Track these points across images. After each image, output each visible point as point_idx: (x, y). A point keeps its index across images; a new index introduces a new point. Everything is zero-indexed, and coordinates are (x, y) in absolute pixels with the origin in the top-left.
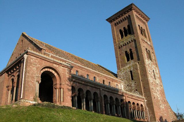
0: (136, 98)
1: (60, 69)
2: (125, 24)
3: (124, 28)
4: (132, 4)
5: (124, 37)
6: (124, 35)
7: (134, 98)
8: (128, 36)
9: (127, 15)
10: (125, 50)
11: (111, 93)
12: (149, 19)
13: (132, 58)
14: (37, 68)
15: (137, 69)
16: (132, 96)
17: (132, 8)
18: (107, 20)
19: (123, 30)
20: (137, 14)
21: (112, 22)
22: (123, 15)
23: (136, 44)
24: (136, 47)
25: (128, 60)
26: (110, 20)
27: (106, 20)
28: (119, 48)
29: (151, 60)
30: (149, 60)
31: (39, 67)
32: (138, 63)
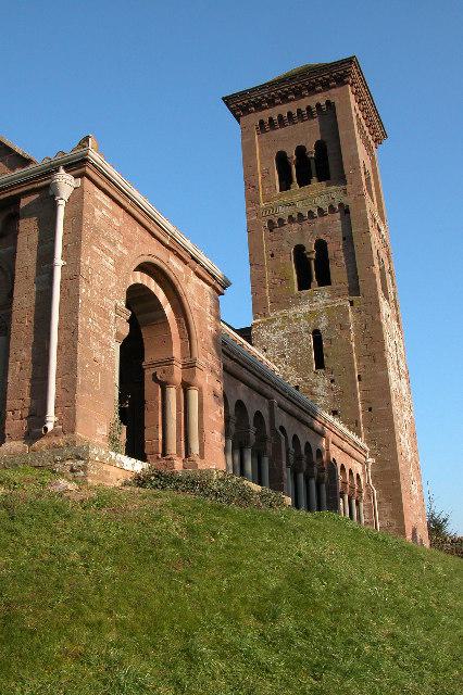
0: (349, 448)
1: (193, 290)
2: (308, 135)
3: (301, 151)
4: (350, 61)
5: (295, 185)
6: (295, 180)
7: (345, 445)
8: (316, 185)
9: (321, 99)
10: (298, 242)
11: (296, 421)
12: (385, 135)
13: (325, 280)
14: (119, 263)
15: (344, 327)
17: (347, 74)
18: (228, 100)
19: (292, 154)
21: (249, 113)
22: (304, 96)
23: (347, 225)
24: (348, 239)
25: (304, 283)
26: (240, 105)
27: (223, 99)
28: (265, 226)
29: (388, 299)
32: (352, 303)
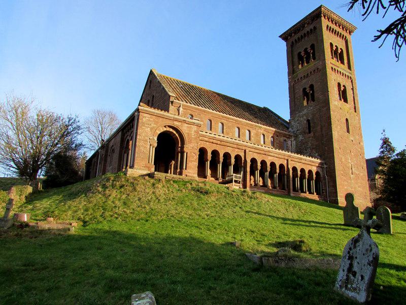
14: (151, 129)
16: (301, 159)
17: (320, 13)
20: (330, 24)
30: (342, 100)
31: (154, 127)
